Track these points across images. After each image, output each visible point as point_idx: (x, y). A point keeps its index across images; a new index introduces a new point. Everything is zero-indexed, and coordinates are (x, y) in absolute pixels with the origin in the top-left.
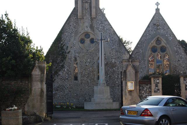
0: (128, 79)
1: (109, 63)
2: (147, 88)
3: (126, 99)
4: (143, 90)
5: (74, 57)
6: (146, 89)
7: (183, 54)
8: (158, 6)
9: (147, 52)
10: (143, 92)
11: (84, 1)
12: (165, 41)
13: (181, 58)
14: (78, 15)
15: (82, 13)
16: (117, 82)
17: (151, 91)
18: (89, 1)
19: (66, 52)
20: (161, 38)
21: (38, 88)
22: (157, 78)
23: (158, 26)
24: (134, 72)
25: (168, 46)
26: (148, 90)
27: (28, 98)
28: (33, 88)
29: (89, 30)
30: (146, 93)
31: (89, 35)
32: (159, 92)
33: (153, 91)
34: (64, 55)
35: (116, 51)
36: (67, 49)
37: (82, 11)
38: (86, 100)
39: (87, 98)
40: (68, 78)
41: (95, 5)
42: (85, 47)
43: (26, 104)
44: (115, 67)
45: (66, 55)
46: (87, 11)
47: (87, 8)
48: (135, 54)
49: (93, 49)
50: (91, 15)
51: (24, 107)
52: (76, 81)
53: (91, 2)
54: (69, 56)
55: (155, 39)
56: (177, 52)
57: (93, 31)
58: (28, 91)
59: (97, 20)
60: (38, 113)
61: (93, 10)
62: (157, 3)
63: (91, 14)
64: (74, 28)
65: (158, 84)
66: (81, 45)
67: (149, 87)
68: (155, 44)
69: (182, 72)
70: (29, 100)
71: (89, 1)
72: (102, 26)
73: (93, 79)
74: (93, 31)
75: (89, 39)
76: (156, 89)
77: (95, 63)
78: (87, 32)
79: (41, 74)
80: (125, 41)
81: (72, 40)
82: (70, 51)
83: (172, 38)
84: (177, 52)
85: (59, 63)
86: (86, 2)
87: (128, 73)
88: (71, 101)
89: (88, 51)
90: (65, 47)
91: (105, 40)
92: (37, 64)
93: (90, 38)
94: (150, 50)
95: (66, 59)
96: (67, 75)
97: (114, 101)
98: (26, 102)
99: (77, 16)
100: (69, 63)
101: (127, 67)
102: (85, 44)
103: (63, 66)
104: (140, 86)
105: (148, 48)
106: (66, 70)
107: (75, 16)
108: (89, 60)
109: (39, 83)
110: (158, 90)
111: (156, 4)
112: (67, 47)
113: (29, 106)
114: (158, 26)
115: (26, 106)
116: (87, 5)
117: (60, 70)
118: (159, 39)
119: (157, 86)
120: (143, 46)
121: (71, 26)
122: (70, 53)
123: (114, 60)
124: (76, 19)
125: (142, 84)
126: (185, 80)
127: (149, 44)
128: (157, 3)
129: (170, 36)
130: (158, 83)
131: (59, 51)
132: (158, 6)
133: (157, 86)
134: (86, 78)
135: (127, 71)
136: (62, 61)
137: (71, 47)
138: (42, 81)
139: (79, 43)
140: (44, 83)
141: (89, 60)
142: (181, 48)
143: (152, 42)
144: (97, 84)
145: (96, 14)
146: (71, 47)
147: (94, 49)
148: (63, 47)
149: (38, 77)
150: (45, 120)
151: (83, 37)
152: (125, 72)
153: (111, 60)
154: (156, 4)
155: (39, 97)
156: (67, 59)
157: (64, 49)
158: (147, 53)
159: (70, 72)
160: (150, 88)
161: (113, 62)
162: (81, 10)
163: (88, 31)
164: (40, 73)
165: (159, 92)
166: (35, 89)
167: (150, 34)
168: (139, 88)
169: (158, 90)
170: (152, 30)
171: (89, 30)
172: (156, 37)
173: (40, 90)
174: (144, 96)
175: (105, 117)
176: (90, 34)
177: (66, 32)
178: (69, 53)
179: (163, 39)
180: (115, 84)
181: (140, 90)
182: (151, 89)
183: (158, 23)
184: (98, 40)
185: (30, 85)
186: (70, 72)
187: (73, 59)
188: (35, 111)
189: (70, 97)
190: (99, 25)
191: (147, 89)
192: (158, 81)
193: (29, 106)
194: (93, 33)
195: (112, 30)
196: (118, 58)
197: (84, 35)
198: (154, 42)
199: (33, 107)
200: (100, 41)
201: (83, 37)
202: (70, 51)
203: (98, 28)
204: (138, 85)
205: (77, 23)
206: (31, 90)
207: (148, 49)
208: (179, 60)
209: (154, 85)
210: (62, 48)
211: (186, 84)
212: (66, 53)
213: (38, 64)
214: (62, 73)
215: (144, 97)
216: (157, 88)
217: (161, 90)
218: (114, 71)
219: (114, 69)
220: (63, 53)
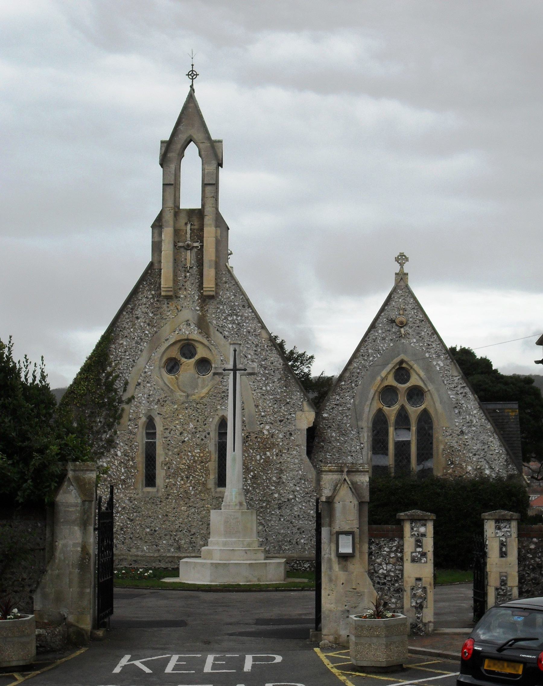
0: (337, 521)
1: (252, 434)
2: (391, 548)
3: (331, 580)
4: (379, 555)
5: (145, 415)
6: (391, 552)
7: (475, 412)
8: (402, 265)
9: (368, 403)
10: (378, 561)
11: (180, 244)
12: (422, 374)
13: (470, 424)
14: (160, 284)
15: (175, 281)
16: (276, 495)
17: (402, 559)
18: (196, 244)
19: (120, 399)
20: (412, 363)
21: (75, 545)
22: (420, 520)
23: (402, 325)
24: (356, 503)
25: (431, 387)
26: (392, 555)
27: (43, 572)
28: (60, 544)
29: (195, 334)
30: (387, 564)
31: (194, 348)
32: (425, 563)
33: (407, 557)
34: (116, 409)
35: (276, 400)
36: (125, 390)
37: (175, 275)
38: (180, 547)
39: (183, 542)
40: (128, 477)
41: (214, 258)
42: (180, 383)
43: (39, 590)
44: (270, 449)
45: (123, 410)
46: (188, 274)
47: (188, 265)
48: (333, 408)
49: (205, 391)
50: (201, 286)
51: (31, 598)
52: (149, 489)
53: (202, 246)
54: (130, 410)
55: (390, 366)
56: (457, 405)
57: (208, 336)
58: (44, 549)
59: (221, 303)
60: (71, 619)
61: (209, 273)
62: (402, 255)
63: (202, 283)
64: (149, 325)
65: (424, 539)
66: (168, 377)
67: (398, 547)
68: (391, 381)
69: (469, 468)
70: (46, 578)
71: (196, 244)
72: (233, 322)
73: (204, 484)
74: (208, 336)
75: (193, 361)
76: (416, 552)
77: (209, 434)
78: (187, 339)
79: (84, 502)
80: (292, 353)
81: (141, 361)
82: (133, 397)
83: (442, 365)
84: (457, 405)
85: (98, 432)
86: (188, 248)
87: (338, 506)
88: (135, 550)
89: (190, 398)
90: (118, 385)
91: (245, 370)
92: (70, 474)
93: (197, 357)
94: (376, 397)
95: (122, 421)
96: (123, 470)
97: (117, 389)
98: (38, 583)
99: (159, 288)
100: (131, 432)
101: (335, 490)
102: (181, 377)
103: (111, 443)
104: (370, 543)
105: (372, 392)
106: (119, 453)
107: (150, 290)
108: (191, 426)
109: (76, 528)
110: (424, 554)
111: (397, 260)
112: (126, 383)
113: (45, 596)
114: (402, 325)
115: (37, 597)
116: (189, 257)
117: (102, 453)
118: (404, 365)
119: (419, 543)
120: (356, 385)
121: (137, 318)
122: (135, 403)
123: (267, 427)
124: (153, 298)
125: (376, 536)
126: (499, 529)
127: (373, 378)
128: (402, 255)
129: (439, 356)
130: (424, 535)
131: (101, 397)
132: (402, 265)
133: (419, 543)
134: (182, 480)
135: (337, 499)
136: (110, 426)
137: (139, 384)
138: (84, 525)
139: (164, 372)
140: (91, 528)
141: (191, 426)
142: (470, 395)
143: (383, 374)
144: (218, 505)
145: (217, 285)
146: (139, 384)
147: (208, 393)
148: (112, 383)
149: (75, 513)
150: (94, 638)
151: (175, 353)
152: (330, 502)
153: (258, 428)
154: (397, 260)
155: (77, 571)
156: (124, 420)
157: (116, 391)
158: (367, 409)
159: (133, 459)
160: (400, 548)
161: (266, 432)
162: (171, 270)
163: (191, 337)
164: (79, 501)
165: (426, 562)
166: (65, 546)
167: (378, 351)
168: (370, 548)
169: (424, 554)
170: (384, 339)
171: (195, 334)
172: (397, 360)
173: (79, 549)
174: (381, 571)
175: (259, 622)
176: (197, 345)
177: (122, 338)
178: (130, 400)
179: (415, 366)
180: (268, 502)
181: (370, 554)
182: (402, 552)
183: (403, 319)
184: (224, 370)
185: (48, 535)
186: (133, 459)
187: (144, 419)
188: (64, 611)
189: (131, 538)
190: (226, 318)
191: (392, 552)
192: (422, 530)
193: (45, 596)
194: (205, 341)
195: (264, 335)
196: (281, 421)
197: (178, 345)
198: (388, 373)
199: (59, 598)
200: (232, 372)
201: (175, 353)
202: (133, 397)
203: (221, 329)
204: (366, 540)
205: (157, 311)
206: (53, 548)
207: (371, 396)
208: (462, 433)
209: (413, 540)
210: (110, 387)
211: (501, 539)
212: (120, 401)
213: (74, 471)
214: (108, 462)
215: (383, 574)
216: (419, 549)
217: (430, 555)
218: (267, 461)
219: (268, 453)
220: (113, 400)
